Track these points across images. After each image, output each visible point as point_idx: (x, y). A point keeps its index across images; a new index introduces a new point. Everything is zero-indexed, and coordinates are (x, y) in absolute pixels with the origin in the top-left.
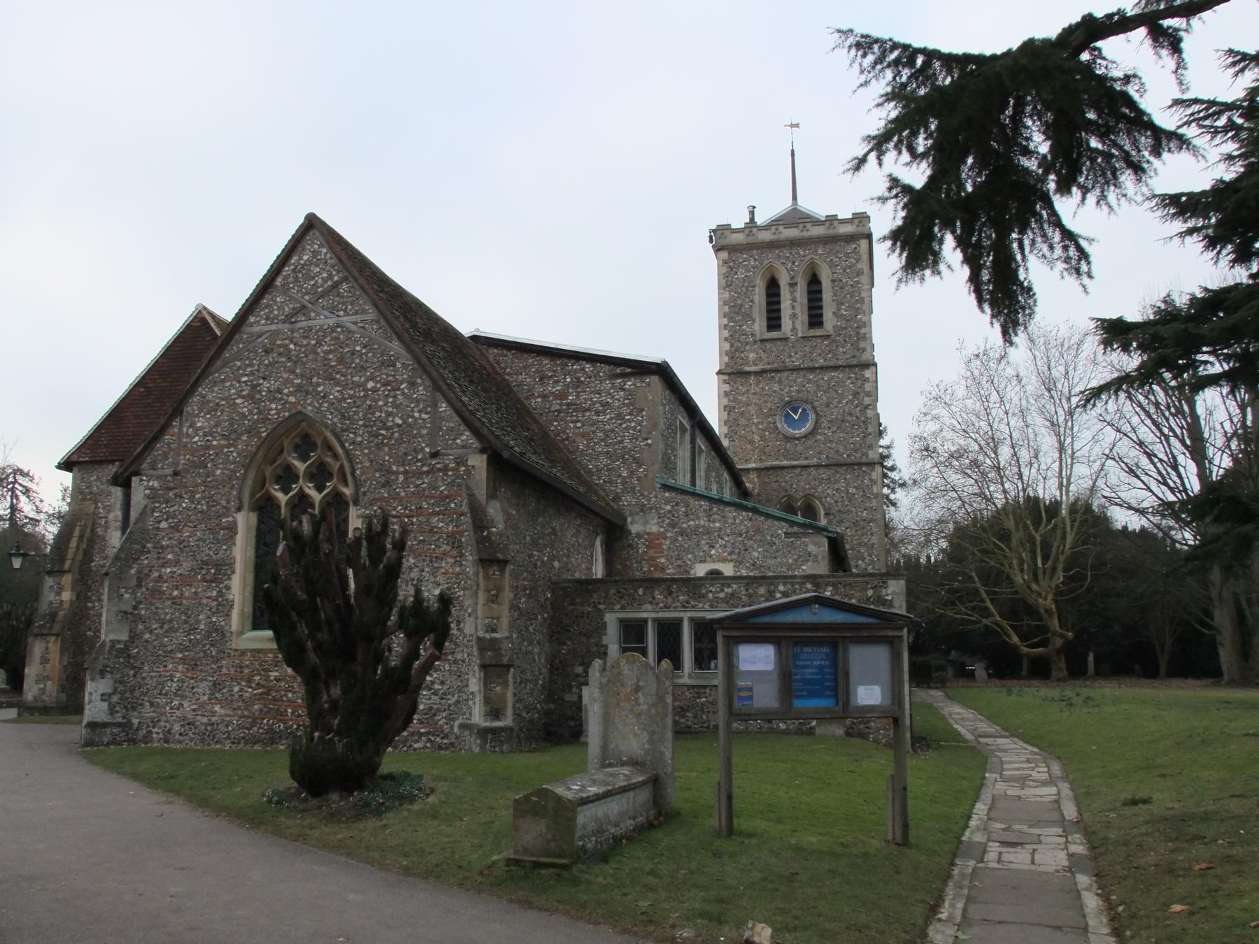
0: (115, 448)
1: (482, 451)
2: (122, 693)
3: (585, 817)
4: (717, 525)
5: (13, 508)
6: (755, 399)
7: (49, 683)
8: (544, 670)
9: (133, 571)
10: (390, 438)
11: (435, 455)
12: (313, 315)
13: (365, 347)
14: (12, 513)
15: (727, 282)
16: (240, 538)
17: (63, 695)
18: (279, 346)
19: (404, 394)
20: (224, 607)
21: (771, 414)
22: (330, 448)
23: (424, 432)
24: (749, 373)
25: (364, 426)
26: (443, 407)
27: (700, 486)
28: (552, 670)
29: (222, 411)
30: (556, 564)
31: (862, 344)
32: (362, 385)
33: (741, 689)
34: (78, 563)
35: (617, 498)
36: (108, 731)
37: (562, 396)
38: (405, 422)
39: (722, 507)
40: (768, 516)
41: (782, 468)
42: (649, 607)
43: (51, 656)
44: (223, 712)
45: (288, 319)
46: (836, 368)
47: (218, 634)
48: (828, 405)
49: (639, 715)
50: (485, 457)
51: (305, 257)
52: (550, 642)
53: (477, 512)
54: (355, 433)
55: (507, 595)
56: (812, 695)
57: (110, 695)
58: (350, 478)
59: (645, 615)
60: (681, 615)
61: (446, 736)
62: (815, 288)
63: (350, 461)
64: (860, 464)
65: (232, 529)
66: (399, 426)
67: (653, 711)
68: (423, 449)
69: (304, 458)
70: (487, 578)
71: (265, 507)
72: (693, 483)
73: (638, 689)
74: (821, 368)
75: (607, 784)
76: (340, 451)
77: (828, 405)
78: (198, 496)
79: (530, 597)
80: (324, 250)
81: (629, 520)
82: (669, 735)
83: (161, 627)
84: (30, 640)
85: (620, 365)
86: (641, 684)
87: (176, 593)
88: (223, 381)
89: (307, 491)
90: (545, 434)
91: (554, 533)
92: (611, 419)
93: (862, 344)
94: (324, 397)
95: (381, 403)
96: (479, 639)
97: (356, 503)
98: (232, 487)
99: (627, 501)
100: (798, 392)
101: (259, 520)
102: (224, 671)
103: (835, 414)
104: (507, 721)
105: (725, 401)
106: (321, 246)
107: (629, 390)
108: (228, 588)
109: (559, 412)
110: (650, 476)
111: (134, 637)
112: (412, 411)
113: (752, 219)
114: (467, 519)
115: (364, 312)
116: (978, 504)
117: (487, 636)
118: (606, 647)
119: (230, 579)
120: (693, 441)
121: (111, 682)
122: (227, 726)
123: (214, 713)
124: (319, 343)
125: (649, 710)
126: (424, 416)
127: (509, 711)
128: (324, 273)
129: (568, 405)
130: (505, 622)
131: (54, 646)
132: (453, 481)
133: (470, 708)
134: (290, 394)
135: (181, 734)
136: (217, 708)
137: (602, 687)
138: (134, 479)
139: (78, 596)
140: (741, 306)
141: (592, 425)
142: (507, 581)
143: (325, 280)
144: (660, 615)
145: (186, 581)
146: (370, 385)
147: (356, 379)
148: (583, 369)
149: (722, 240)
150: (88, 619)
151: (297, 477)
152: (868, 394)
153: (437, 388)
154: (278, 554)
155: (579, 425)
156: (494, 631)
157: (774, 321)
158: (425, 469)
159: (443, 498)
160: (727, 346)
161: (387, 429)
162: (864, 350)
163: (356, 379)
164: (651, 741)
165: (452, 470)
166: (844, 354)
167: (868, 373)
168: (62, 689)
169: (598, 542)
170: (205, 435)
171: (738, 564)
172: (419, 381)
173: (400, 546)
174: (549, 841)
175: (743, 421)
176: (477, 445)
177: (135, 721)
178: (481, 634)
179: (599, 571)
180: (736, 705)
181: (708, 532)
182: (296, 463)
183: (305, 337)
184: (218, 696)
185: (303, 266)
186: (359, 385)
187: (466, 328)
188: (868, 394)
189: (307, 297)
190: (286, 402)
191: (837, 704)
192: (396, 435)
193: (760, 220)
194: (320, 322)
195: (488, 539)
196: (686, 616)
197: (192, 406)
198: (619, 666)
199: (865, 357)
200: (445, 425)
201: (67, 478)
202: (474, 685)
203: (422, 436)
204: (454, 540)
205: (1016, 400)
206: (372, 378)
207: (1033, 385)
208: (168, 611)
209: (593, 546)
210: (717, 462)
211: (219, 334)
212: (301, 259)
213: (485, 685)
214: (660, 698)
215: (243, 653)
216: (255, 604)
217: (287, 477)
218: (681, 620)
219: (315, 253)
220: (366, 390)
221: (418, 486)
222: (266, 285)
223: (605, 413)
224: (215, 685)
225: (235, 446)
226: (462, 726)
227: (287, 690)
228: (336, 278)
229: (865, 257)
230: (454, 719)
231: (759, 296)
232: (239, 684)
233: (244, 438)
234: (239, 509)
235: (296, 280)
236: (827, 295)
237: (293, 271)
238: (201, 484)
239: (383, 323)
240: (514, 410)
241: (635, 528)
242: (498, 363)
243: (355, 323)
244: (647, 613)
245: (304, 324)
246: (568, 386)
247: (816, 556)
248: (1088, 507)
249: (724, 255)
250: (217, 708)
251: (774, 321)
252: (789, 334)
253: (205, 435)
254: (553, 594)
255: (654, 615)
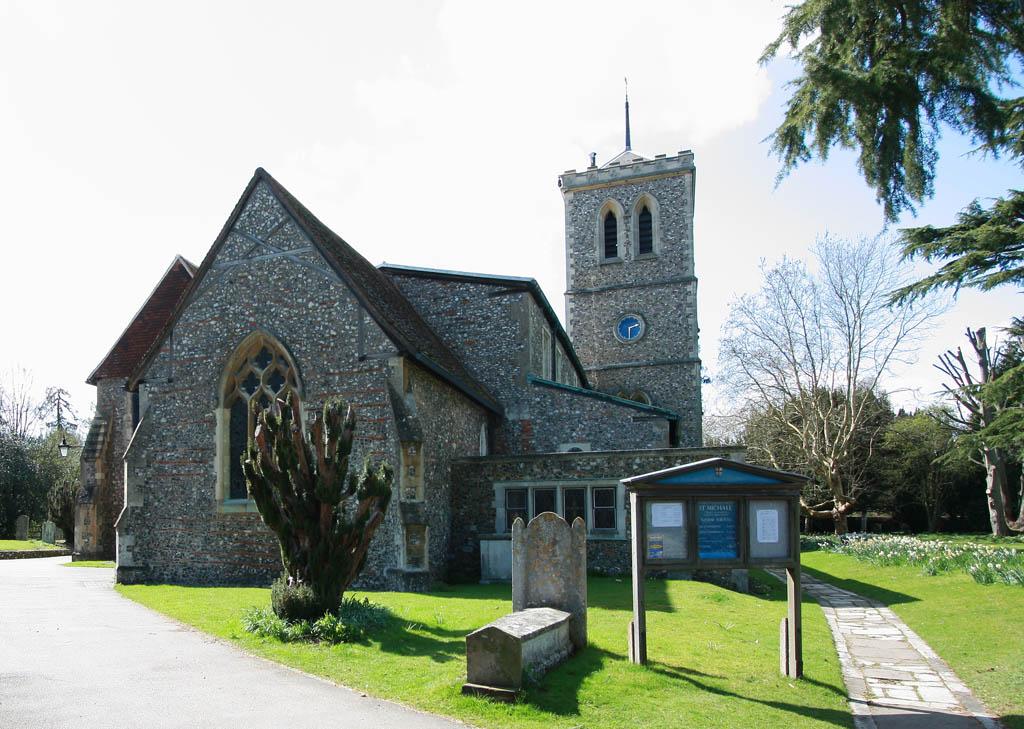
0: (128, 364)
1: (400, 354)
2: (141, 546)
3: (526, 649)
4: (578, 412)
5: (59, 418)
6: (596, 314)
7: (91, 538)
8: (447, 528)
9: (144, 456)
10: (328, 347)
11: (362, 359)
12: (264, 251)
13: (305, 274)
14: (59, 420)
15: (572, 219)
16: (219, 429)
17: (101, 547)
18: (241, 277)
19: (336, 310)
20: (210, 481)
21: (609, 324)
22: (282, 357)
23: (353, 340)
24: (590, 293)
25: (307, 338)
26: (368, 319)
27: (559, 381)
28: (453, 527)
29: (201, 331)
30: (454, 445)
31: (685, 264)
32: (305, 306)
33: (652, 543)
34: (104, 453)
35: (496, 393)
36: (133, 572)
37: (452, 312)
38: (338, 333)
39: (581, 398)
40: (619, 404)
41: (617, 368)
42: (528, 478)
43: (91, 519)
44: (212, 559)
45: (247, 256)
46: (663, 284)
47: (206, 502)
48: (655, 316)
49: (555, 565)
50: (402, 359)
51: (257, 205)
52: (451, 506)
53: (397, 403)
54: (300, 344)
55: (421, 470)
56: (717, 547)
57: (133, 547)
58: (298, 380)
59: (526, 484)
60: (555, 483)
61: (377, 579)
62: (646, 218)
63: (298, 366)
64: (681, 363)
65: (213, 422)
66: (333, 336)
67: (568, 561)
68: (353, 354)
69: (263, 367)
70: (407, 455)
71: (237, 408)
72: (554, 378)
73: (555, 543)
74: (650, 285)
75: (539, 624)
76: (290, 358)
77: (655, 316)
78: (186, 398)
79: (436, 471)
80: (271, 198)
81: (506, 410)
82: (584, 581)
83: (166, 496)
84: (77, 508)
85: (497, 285)
86: (557, 539)
87: (174, 471)
88: (200, 308)
89: (266, 391)
90: (438, 340)
91: (452, 420)
92: (491, 329)
93: (685, 264)
94: (276, 316)
95: (319, 319)
96: (402, 504)
97: (304, 398)
98: (211, 390)
99: (504, 395)
100: (631, 306)
101: (231, 414)
102: (212, 529)
103: (662, 322)
104: (425, 568)
105: (571, 316)
106: (268, 195)
107: (506, 306)
108: (212, 467)
109: (450, 325)
110: (523, 375)
111: (147, 504)
112: (344, 324)
113: (594, 164)
114: (389, 409)
115: (303, 246)
116: (774, 394)
117: (408, 501)
118: (495, 510)
119: (212, 460)
120: (553, 346)
121: (133, 538)
122: (216, 570)
123: (206, 561)
124: (271, 273)
125: (564, 560)
126: (353, 328)
127: (426, 560)
128: (272, 215)
129: (456, 319)
130: (421, 491)
131: (93, 514)
132: (377, 379)
133: (395, 557)
134: (251, 315)
135: (184, 576)
136: (208, 557)
137: (523, 542)
138: (141, 386)
139: (106, 476)
140: (585, 237)
141: (476, 336)
142: (422, 459)
143: (272, 222)
144: (538, 484)
145: (181, 462)
146: (311, 305)
147: (300, 300)
148: (468, 290)
149: (568, 182)
150: (114, 492)
151: (259, 381)
152: (690, 305)
153: (362, 305)
154: (256, 435)
155: (465, 335)
156: (414, 497)
157: (611, 249)
158: (355, 370)
159: (368, 393)
160: (573, 271)
161: (325, 339)
162: (687, 268)
163: (300, 300)
164: (567, 587)
165: (376, 370)
166: (669, 271)
167: (689, 288)
168: (100, 543)
169: (483, 428)
170: (190, 350)
171: (595, 444)
172: (348, 300)
173: (351, 426)
174: (498, 673)
175: (585, 332)
176: (394, 349)
177: (152, 566)
178: (403, 499)
179: (483, 451)
180: (649, 555)
181: (570, 418)
182: (258, 370)
183: (259, 269)
184: (209, 547)
185: (256, 211)
186: (299, 306)
187: (376, 262)
188: (690, 305)
189: (259, 237)
190: (248, 321)
191: (739, 556)
192: (332, 344)
193: (600, 164)
194: (271, 256)
195: (406, 424)
196: (589, 484)
197: (178, 329)
198: (538, 524)
199: (687, 274)
200: (370, 335)
201: (94, 389)
202: (399, 540)
203: (352, 344)
204: (379, 425)
205: (810, 306)
206: (312, 299)
207: (826, 292)
208: (169, 485)
209: (479, 431)
210: (569, 363)
211: (192, 276)
212: (253, 206)
213: (407, 540)
214: (575, 550)
215: (225, 516)
216: (231, 479)
217: (251, 382)
218: (586, 488)
219: (264, 201)
220: (307, 309)
221: (350, 384)
222: (229, 229)
223: (485, 324)
224: (206, 540)
225: (212, 358)
226: (388, 571)
227: (257, 543)
228: (281, 220)
229: (689, 189)
230: (383, 567)
231: (598, 228)
232: (223, 539)
233: (218, 351)
234: (217, 407)
235: (251, 223)
236: (655, 225)
237: (248, 216)
238: (188, 389)
239: (318, 254)
240: (425, 320)
241: (511, 417)
242: (402, 289)
243: (297, 255)
244: (527, 483)
245: (259, 258)
246: (456, 304)
247: (659, 436)
248: (871, 396)
249: (571, 196)
250: (208, 557)
251: (611, 249)
252: (623, 258)
253: (190, 350)
254: (452, 468)
255: (532, 484)
